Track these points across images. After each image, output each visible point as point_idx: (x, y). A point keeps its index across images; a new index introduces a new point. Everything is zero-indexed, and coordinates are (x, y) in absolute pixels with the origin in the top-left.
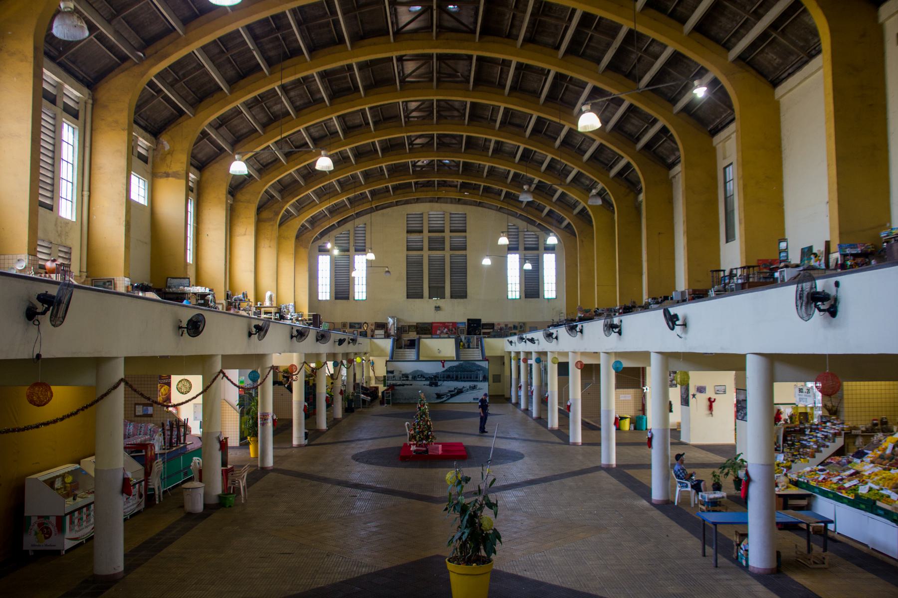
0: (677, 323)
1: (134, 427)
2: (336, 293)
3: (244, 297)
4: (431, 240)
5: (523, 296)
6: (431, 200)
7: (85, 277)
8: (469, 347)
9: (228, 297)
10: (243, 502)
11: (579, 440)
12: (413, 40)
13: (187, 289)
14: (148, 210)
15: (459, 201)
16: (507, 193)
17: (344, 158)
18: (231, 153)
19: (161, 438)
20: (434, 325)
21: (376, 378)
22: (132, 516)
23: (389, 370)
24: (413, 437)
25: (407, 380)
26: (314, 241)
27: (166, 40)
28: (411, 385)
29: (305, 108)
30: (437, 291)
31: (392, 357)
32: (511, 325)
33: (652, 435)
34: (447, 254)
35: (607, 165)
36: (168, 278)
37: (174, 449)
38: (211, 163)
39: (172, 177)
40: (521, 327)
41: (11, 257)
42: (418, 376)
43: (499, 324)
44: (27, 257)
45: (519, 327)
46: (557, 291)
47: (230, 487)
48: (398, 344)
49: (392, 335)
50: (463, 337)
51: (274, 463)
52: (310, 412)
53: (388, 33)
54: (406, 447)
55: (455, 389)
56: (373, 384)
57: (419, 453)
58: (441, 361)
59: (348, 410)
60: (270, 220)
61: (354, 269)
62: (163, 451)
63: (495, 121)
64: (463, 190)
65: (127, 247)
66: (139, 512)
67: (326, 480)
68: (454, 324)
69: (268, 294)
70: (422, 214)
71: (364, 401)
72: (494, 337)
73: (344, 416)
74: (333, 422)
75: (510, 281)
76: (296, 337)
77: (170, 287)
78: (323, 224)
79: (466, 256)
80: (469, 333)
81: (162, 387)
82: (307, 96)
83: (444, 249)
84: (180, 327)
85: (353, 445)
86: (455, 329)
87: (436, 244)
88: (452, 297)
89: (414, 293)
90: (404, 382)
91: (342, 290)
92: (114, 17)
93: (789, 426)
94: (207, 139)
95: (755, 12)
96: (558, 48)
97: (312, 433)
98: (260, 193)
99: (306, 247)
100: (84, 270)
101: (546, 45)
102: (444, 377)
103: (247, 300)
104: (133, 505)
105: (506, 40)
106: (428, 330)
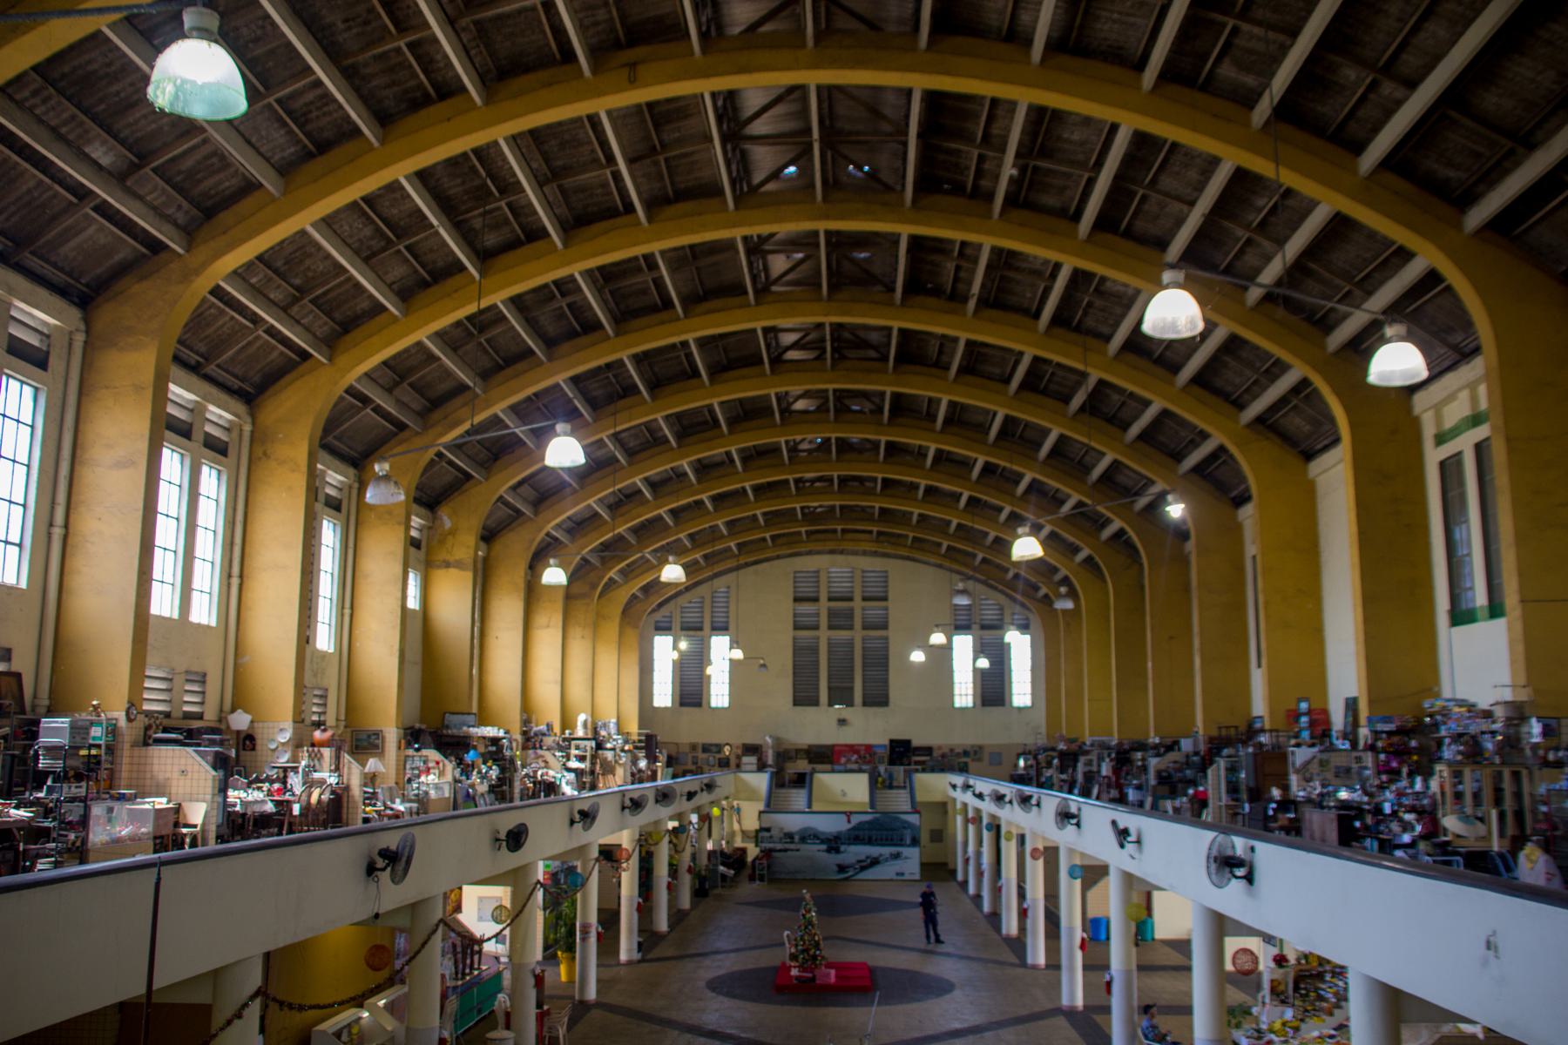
0: (1129, 839)
1: (406, 940)
3: (548, 730)
4: (832, 614)
5: (979, 702)
6: (832, 552)
7: (342, 728)
8: (891, 787)
9: (524, 733)
12: (797, 371)
13: (473, 730)
14: (420, 616)
15: (875, 554)
16: (971, 500)
20: (837, 748)
21: (743, 832)
23: (764, 825)
24: (793, 957)
27: (458, 401)
28: (798, 850)
29: (644, 450)
30: (841, 694)
31: (768, 804)
33: (1111, 978)
34: (857, 635)
36: (445, 713)
37: (468, 978)
38: (505, 531)
39: (454, 567)
40: (975, 753)
41: (271, 725)
42: (808, 836)
43: (940, 748)
44: (291, 726)
45: (972, 753)
46: (1034, 694)
49: (770, 766)
50: (882, 769)
51: (598, 992)
52: (645, 909)
53: (761, 362)
54: (785, 969)
56: (739, 843)
58: (845, 813)
59: (700, 893)
61: (709, 663)
65: (400, 685)
67: (670, 1023)
68: (869, 748)
69: (582, 718)
70: (818, 572)
71: (724, 877)
72: (933, 770)
73: (694, 905)
74: (677, 917)
75: (957, 677)
77: (448, 727)
79: (886, 638)
80: (892, 762)
84: (497, 840)
85: (707, 962)
87: (840, 620)
88: (865, 704)
89: (804, 697)
90: (787, 846)
91: (691, 692)
92: (397, 384)
93: (1303, 968)
95: (1267, 371)
96: (1007, 381)
97: (648, 939)
99: (636, 627)
100: (343, 717)
101: (990, 378)
102: (849, 839)
105: (934, 371)
106: (826, 756)
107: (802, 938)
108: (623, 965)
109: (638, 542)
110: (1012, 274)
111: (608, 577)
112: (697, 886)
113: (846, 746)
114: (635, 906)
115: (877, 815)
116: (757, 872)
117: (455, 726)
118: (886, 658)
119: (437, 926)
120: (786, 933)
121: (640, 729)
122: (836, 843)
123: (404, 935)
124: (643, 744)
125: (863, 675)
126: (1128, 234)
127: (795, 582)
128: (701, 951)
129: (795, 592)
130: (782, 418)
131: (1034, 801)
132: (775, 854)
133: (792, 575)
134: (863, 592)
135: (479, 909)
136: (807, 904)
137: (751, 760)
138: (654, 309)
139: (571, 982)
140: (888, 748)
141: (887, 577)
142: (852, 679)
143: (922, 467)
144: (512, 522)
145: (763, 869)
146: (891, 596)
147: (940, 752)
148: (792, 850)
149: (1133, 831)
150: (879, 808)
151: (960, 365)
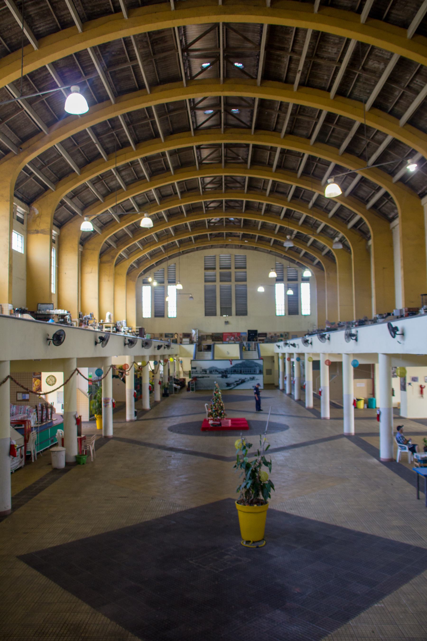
0: (398, 333)
1: (16, 408)
2: (155, 313)
3: (91, 317)
4: (221, 275)
5: (287, 313)
6: (222, 247)
9: (80, 316)
10: (92, 460)
11: (328, 416)
13: (52, 311)
14: (24, 257)
15: (241, 247)
17: (160, 218)
18: (81, 215)
19: (35, 416)
20: (225, 334)
22: (16, 471)
23: (193, 366)
24: (210, 414)
25: (206, 374)
26: (140, 276)
27: (35, 138)
28: (209, 377)
29: (133, 183)
30: (226, 311)
32: (279, 334)
33: (380, 412)
34: (233, 284)
35: (345, 220)
36: (38, 304)
37: (44, 423)
39: (41, 233)
40: (286, 335)
42: (213, 371)
43: (270, 334)
45: (284, 336)
47: (83, 450)
48: (199, 349)
49: (195, 342)
50: (245, 343)
51: (114, 433)
53: (190, 130)
54: (206, 421)
55: (240, 380)
56: (182, 376)
57: (216, 426)
58: (229, 360)
59: (165, 395)
60: (108, 262)
61: (167, 295)
62: (36, 425)
63: (266, 190)
64: (244, 239)
65: (10, 283)
66: (20, 468)
68: (239, 334)
70: (215, 256)
71: (176, 389)
73: (162, 400)
74: (154, 404)
76: (128, 344)
77: (40, 310)
78: (146, 264)
79: (246, 285)
80: (249, 340)
81: (35, 380)
82: (134, 175)
83: (230, 281)
84: (48, 339)
85: (168, 420)
86: (239, 337)
88: (237, 314)
94: (64, 206)
98: (101, 243)
101: (301, 136)
102: (231, 372)
103: (93, 318)
104: (17, 463)
107: (214, 405)
108: (128, 422)
109: (133, 237)
110: (319, 61)
111: (119, 254)
112: (164, 392)
113: (229, 333)
114: (133, 394)
115: (244, 361)
116: (190, 387)
117: (43, 310)
118: (246, 294)
119: (6, 380)
120: (206, 405)
121: (137, 326)
122: (226, 373)
123: (15, 406)
124: (138, 333)
125: (236, 302)
126: (387, 20)
127: (205, 261)
128: (165, 416)
129: (205, 265)
130: (199, 167)
131: (326, 337)
132: (198, 379)
133: (203, 258)
134: (235, 265)
135: (58, 398)
136: (216, 388)
137: (186, 340)
138: (134, 90)
139: (101, 429)
140: (247, 334)
141: (246, 258)
142: (231, 304)
143: (265, 195)
144: (72, 218)
145: (193, 385)
146: (247, 267)
147: (270, 335)
148: (206, 377)
149: (399, 328)
150: (244, 357)
151: (286, 131)
